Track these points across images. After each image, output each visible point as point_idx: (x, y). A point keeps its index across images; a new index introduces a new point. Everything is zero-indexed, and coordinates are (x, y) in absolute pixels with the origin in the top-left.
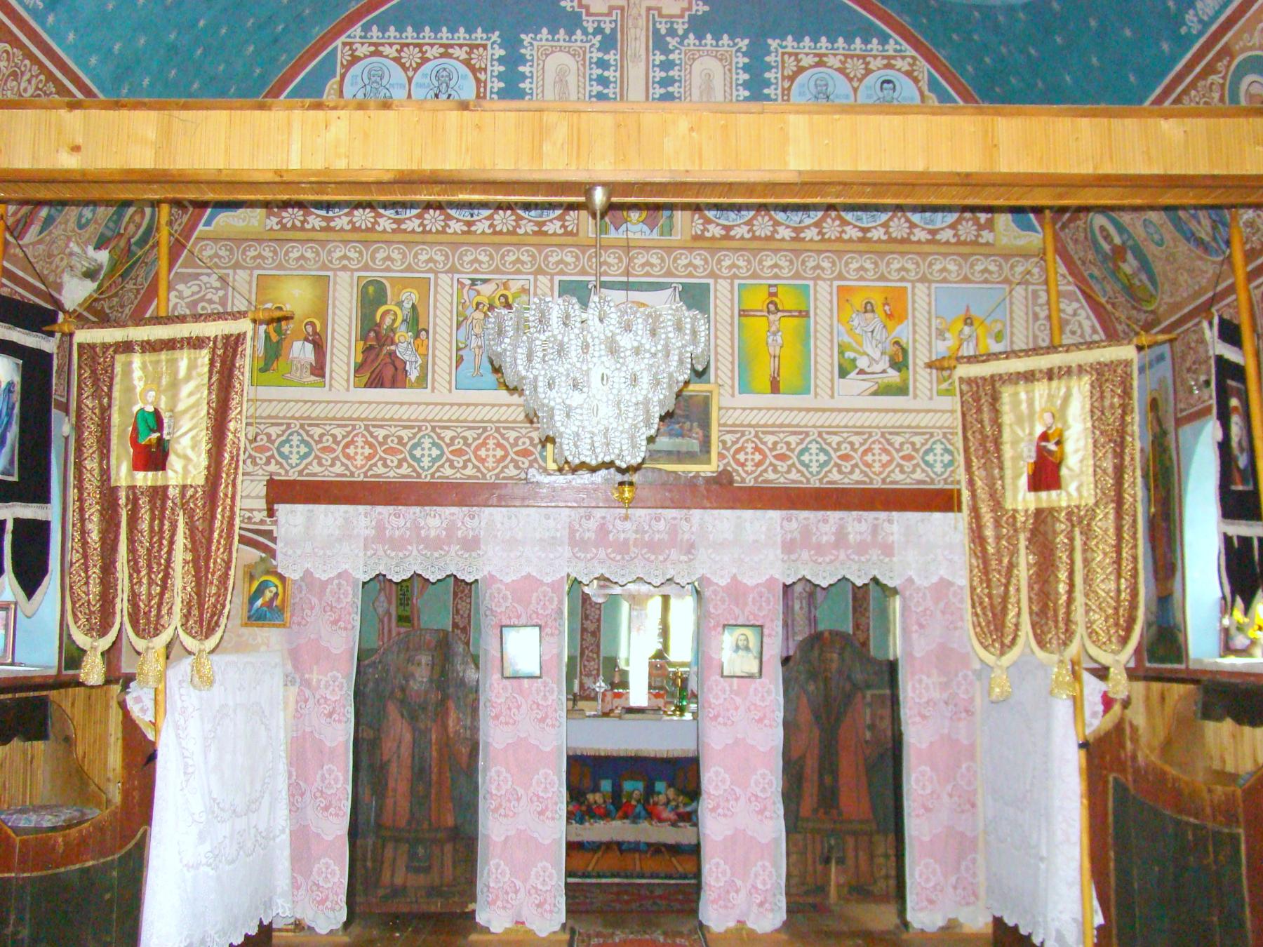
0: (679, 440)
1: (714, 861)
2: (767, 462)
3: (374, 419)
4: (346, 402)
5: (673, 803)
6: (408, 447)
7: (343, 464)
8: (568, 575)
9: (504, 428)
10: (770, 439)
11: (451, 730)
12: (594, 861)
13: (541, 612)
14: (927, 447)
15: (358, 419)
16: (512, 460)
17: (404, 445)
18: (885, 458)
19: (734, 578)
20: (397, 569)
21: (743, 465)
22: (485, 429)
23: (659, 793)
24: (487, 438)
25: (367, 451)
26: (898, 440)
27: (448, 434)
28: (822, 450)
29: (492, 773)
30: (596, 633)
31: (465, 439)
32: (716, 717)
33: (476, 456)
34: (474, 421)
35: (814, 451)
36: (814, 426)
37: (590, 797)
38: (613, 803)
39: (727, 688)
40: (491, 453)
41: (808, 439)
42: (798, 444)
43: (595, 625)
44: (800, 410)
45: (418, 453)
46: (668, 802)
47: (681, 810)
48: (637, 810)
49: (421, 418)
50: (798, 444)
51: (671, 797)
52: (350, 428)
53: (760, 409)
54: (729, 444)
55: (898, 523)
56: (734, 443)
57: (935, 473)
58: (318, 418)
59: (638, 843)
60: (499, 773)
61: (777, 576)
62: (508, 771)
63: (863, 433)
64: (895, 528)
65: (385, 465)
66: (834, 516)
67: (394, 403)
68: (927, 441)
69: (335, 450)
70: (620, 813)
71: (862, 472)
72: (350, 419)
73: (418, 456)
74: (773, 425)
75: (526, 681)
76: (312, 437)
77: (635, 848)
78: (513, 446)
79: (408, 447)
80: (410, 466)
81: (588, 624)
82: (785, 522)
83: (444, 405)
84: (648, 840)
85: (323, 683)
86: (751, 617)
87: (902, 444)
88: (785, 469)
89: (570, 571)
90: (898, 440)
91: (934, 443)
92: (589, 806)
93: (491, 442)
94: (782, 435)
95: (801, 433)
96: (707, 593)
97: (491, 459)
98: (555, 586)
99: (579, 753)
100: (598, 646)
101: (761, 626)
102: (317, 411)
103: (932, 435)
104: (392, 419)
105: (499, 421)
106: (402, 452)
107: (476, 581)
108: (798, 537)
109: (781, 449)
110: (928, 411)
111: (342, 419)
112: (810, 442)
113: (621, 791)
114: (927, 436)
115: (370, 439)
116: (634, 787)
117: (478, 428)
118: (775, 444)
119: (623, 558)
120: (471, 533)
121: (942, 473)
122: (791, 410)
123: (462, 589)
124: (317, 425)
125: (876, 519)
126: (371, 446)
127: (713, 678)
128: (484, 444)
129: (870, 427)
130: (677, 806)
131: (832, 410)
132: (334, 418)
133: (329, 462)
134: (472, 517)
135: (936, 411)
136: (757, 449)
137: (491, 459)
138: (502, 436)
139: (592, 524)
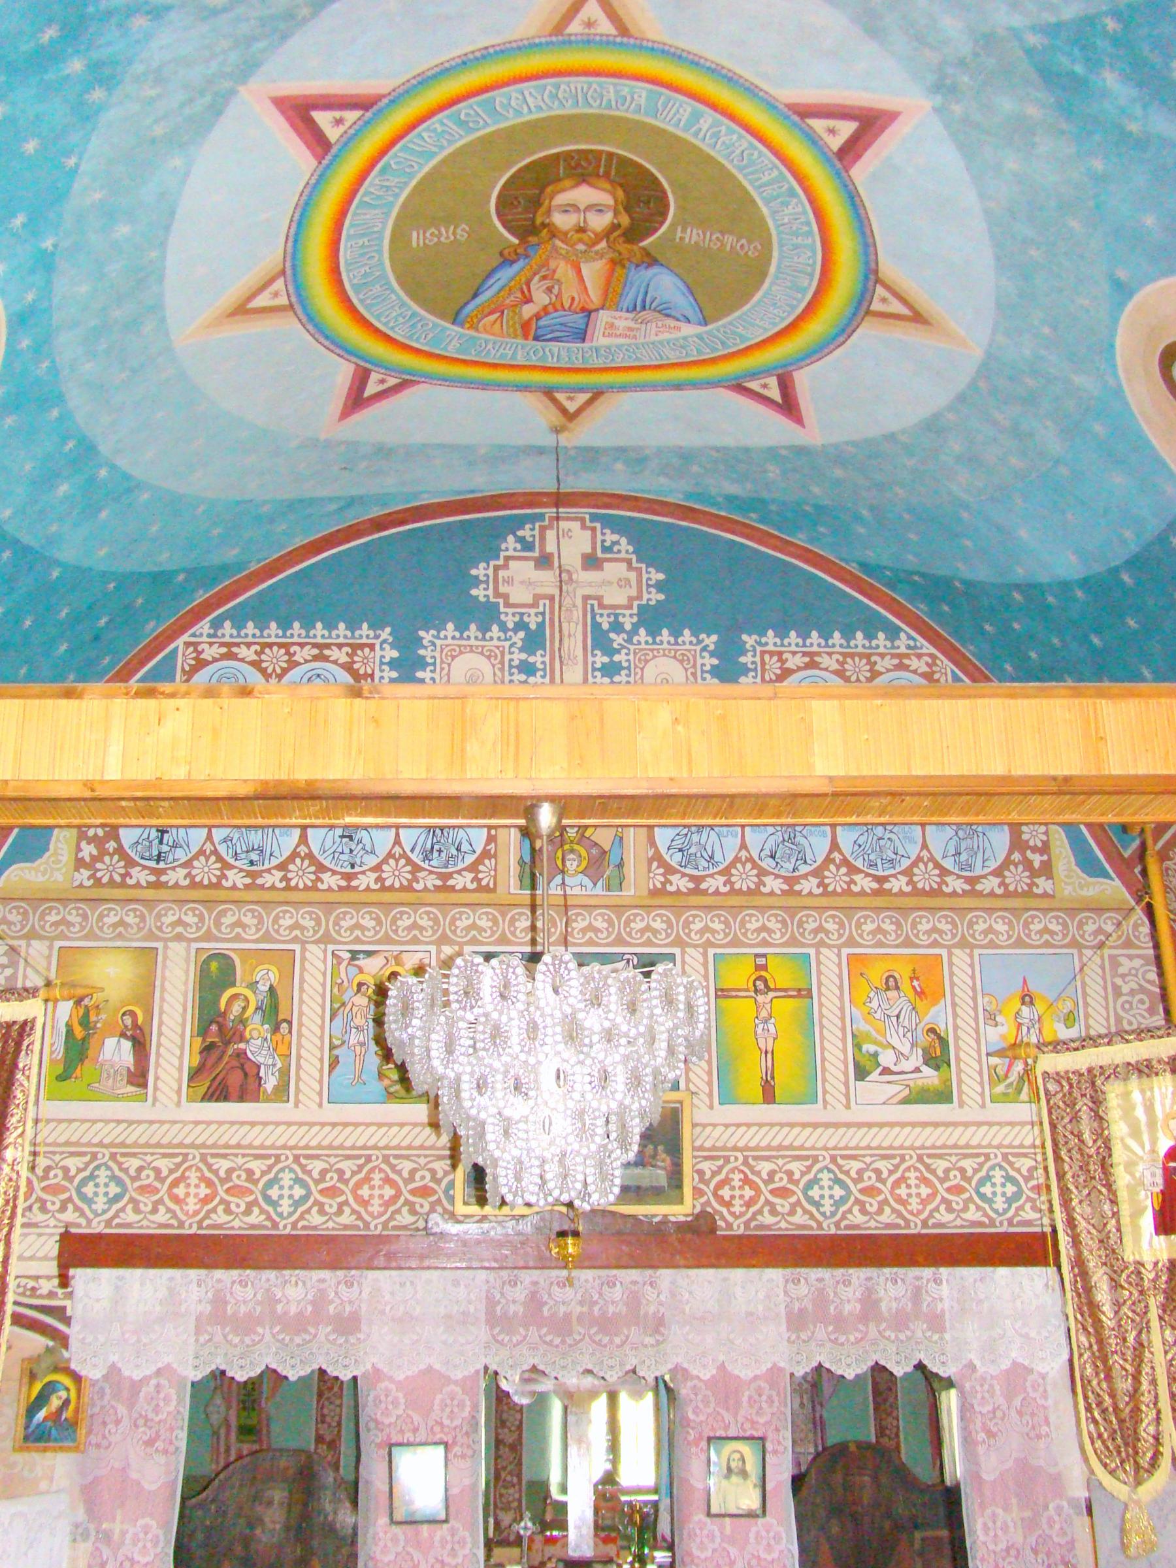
4: (175, 1122)
6: (260, 1185)
9: (396, 1157)
10: (765, 1167)
13: (446, 1422)
18: (925, 1191)
19: (722, 1367)
20: (242, 1362)
21: (728, 1204)
24: (372, 1170)
25: (204, 1191)
26: (940, 1165)
27: (317, 1166)
28: (837, 1181)
30: (516, 1447)
35: (826, 1183)
39: (717, 1533)
40: (377, 1192)
43: (515, 1436)
44: (804, 1125)
45: (274, 1193)
50: (803, 1174)
54: (708, 1175)
55: (949, 1284)
61: (782, 1364)
63: (893, 1157)
64: (945, 1290)
65: (228, 1211)
67: (243, 1123)
68: (981, 1165)
69: (157, 1191)
71: (894, 1210)
72: (181, 1145)
73: (275, 1198)
76: (126, 1171)
85: (129, 1536)
86: (748, 1425)
87: (947, 1171)
90: (940, 1165)
91: (992, 1168)
93: (377, 1177)
94: (780, 1162)
95: (807, 1158)
97: (376, 1202)
100: (520, 1464)
101: (763, 1439)
102: (135, 1135)
103: (987, 1157)
105: (386, 1147)
106: (251, 1192)
108: (810, 1308)
109: (781, 1181)
110: (979, 1124)
111: (170, 1145)
112: (821, 1170)
117: (358, 1157)
118: (772, 1174)
119: (563, 1342)
120: (348, 1309)
122: (792, 1125)
124: (134, 1155)
126: (209, 1183)
128: (367, 1179)
132: (158, 1145)
134: (349, 1284)
136: (746, 1181)
137: (376, 1202)
139: (520, 1293)
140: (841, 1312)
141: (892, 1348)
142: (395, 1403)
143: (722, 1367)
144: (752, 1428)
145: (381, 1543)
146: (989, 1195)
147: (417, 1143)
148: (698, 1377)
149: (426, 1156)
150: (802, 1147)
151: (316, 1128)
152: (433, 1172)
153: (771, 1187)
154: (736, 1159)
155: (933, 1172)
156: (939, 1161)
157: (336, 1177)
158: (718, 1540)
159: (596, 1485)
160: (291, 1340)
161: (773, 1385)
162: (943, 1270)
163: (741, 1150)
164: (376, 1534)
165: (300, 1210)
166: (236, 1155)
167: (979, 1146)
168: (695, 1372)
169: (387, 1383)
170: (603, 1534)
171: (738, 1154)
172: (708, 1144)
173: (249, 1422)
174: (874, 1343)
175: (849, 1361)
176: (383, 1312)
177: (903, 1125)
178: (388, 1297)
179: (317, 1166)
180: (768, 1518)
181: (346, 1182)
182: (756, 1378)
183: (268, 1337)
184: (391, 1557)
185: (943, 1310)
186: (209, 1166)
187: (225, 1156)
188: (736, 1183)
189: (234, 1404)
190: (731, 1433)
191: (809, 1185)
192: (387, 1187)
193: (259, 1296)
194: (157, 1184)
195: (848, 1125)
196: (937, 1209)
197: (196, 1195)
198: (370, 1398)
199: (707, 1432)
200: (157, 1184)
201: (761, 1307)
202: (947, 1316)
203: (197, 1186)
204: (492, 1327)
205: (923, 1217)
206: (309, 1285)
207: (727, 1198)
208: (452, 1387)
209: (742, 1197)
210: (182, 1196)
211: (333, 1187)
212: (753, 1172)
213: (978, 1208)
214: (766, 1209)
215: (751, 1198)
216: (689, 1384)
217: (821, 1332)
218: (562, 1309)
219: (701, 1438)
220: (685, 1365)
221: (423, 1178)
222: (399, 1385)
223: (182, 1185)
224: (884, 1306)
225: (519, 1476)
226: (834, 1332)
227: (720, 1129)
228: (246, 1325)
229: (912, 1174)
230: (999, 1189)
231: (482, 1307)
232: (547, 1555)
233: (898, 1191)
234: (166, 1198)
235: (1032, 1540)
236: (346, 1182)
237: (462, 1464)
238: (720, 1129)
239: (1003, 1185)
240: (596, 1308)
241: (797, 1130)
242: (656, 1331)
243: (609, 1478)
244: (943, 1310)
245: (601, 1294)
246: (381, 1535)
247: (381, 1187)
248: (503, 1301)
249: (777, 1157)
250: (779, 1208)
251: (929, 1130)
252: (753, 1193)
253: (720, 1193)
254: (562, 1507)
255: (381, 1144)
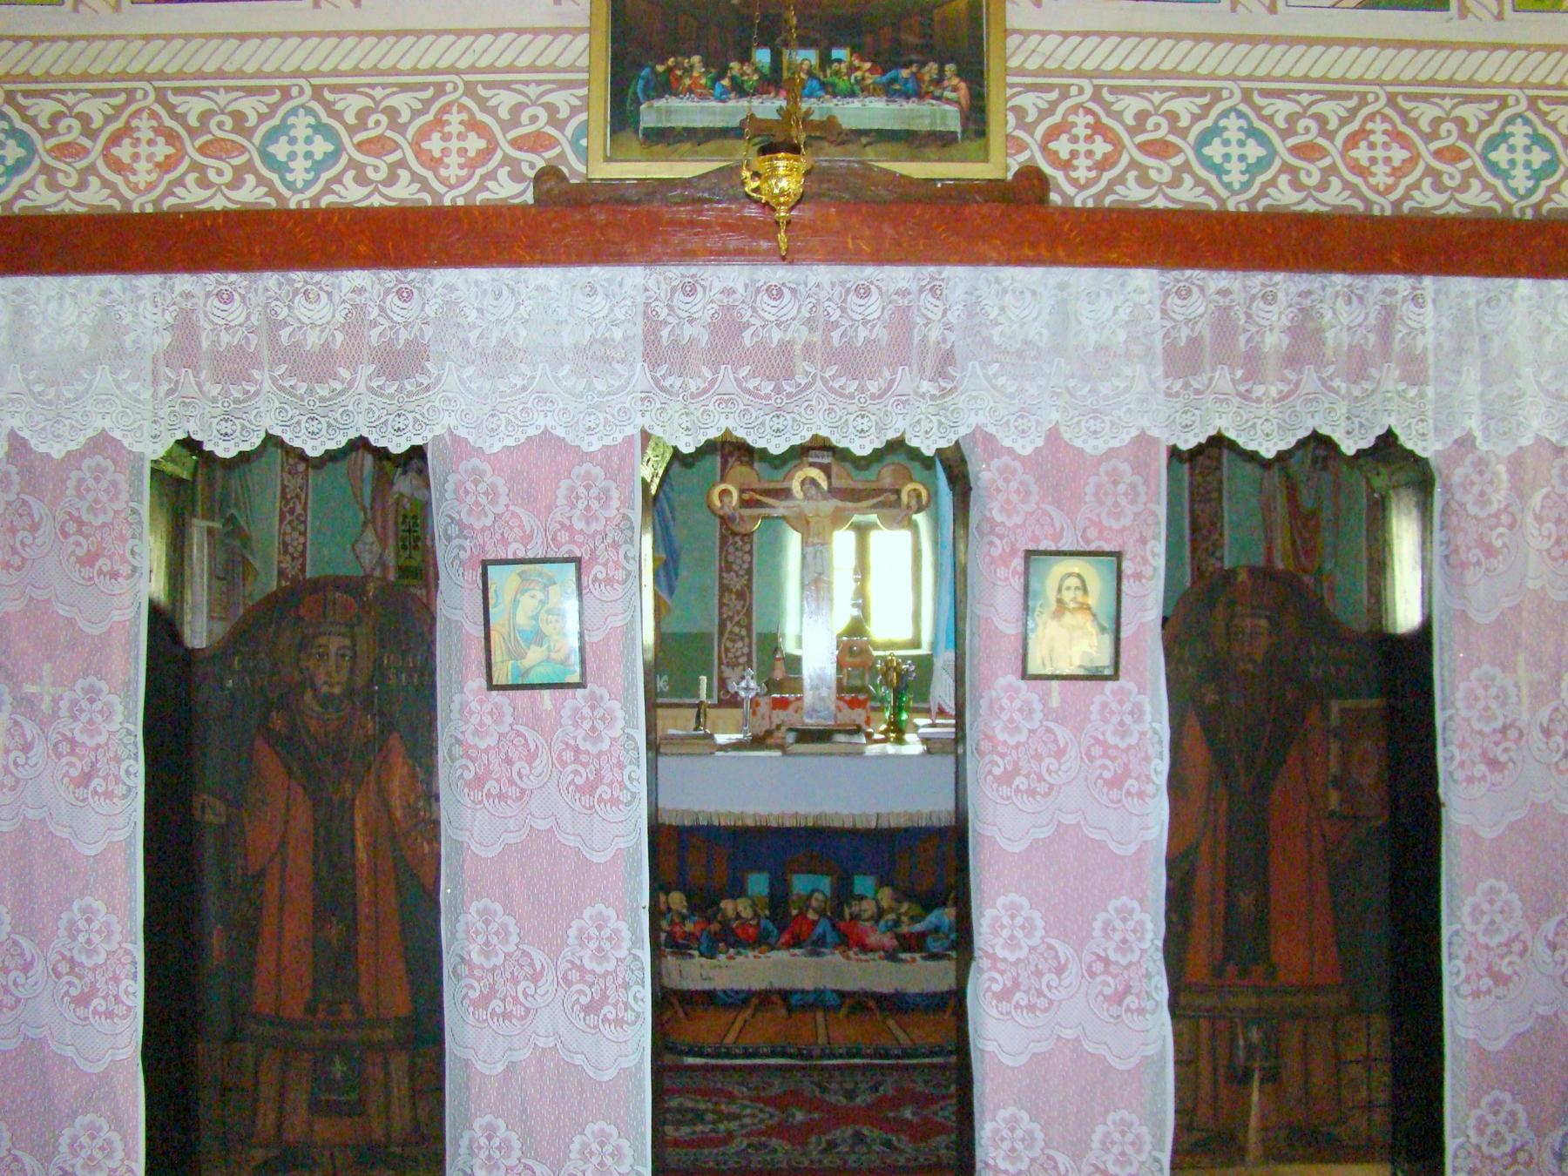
0: (911, 106)
1: (1003, 1114)
2: (1124, 160)
3: (181, 75)
4: (113, 38)
5: (891, 916)
6: (257, 139)
7: (106, 183)
8: (646, 437)
9: (488, 85)
10: (1130, 106)
11: (396, 802)
12: (738, 1025)
13: (579, 525)
14: (1494, 129)
15: (141, 76)
16: (507, 160)
17: (250, 134)
18: (1399, 155)
19: (1053, 436)
20: (226, 427)
21: (1066, 166)
22: (440, 90)
23: (862, 898)
24: (446, 109)
25: (162, 150)
26: (1426, 113)
27: (351, 105)
28: (1252, 132)
29: (472, 915)
30: (744, 594)
31: (393, 113)
32: (1007, 778)
33: (419, 154)
34: (415, 71)
35: (1233, 135)
36: (1232, 77)
37: (727, 906)
38: (772, 919)
39: (1038, 706)
40: (454, 144)
41: (1220, 107)
42: (1196, 118)
43: (744, 581)
44: (1198, 38)
45: (280, 150)
46: (881, 913)
47: (904, 929)
48: (819, 930)
49: (287, 68)
50: (1196, 118)
51: (885, 904)
52: (121, 99)
53: (1104, 35)
54: (1032, 116)
55: (1436, 304)
56: (1044, 114)
57: (1513, 191)
58: (48, 77)
59: (820, 993)
60: (487, 916)
61: (1154, 433)
62: (509, 910)
63: (1348, 96)
64: (1429, 316)
65: (204, 183)
66: (1287, 285)
67: (226, 36)
68: (1492, 115)
69: (87, 151)
70: (786, 937)
71: (1347, 185)
72: (122, 76)
73: (282, 157)
74: (1136, 73)
75: (546, 693)
76: (32, 121)
77: (815, 1002)
78: (506, 126)
79: (257, 139)
80: (261, 181)
81: (730, 578)
82: (1173, 300)
83: (342, 35)
84: (838, 987)
85: (64, 704)
86: (1092, 533)
87: (1436, 122)
88: (1167, 176)
89: (646, 422)
90: (1426, 113)
91: (1510, 121)
92: (725, 924)
93: (455, 119)
94: (1157, 97)
95: (1202, 92)
96: (983, 473)
97: (453, 160)
98: (614, 461)
99: (703, 822)
100: (749, 613)
101: (1118, 555)
102: (46, 60)
103: (1503, 102)
104: (220, 74)
105: (473, 69)
106: (243, 150)
107: (418, 453)
108: (1207, 334)
109: (1158, 129)
110: (1494, 47)
111: (102, 77)
112: (1224, 114)
113: (786, 894)
114: (1494, 105)
115: (169, 122)
116: (811, 886)
117: (423, 87)
118: (1142, 116)
119: (778, 390)
120: (404, 335)
121: (1531, 192)
122: (1178, 37)
123: (392, 479)
124: (45, 94)
125: (1391, 292)
126: (171, 138)
127: (1002, 682)
128: (439, 122)
129: (1360, 81)
130: (897, 923)
131: (1273, 40)
132: (85, 77)
133: (74, 180)
134: (405, 295)
135: (1512, 48)
136: (1098, 128)
137: (453, 160)
138: (482, 103)
139: (703, 308)
140: (1257, 348)
141: (1342, 408)
142: (492, 494)
143: (1053, 436)
144: (1101, 537)
145: (475, 720)
146: (1504, 165)
147: (524, 61)
148: (1010, 451)
149: (539, 83)
150: (1193, 75)
151: (350, 42)
152: (552, 109)
153: (1139, 139)
154: (1081, 91)
155: (1413, 124)
156: (1423, 107)
157: (384, 120)
158: (1038, 715)
159: (839, 636)
160: (311, 391)
161: (1140, 467)
162: (1428, 281)
163: (1089, 76)
164: (464, 705)
165: (325, 176)
166: (215, 90)
167: (1489, 84)
168: (1007, 443)
169: (476, 461)
170: (848, 697)
171: (1085, 83)
172: (1031, 65)
173: (413, 563)
174: (1312, 399)
175: (1267, 427)
176: (465, 343)
177: (1365, 43)
178: (473, 315)
179: (351, 105)
180: (1122, 682)
181: (402, 129)
182: (1111, 453)
183: (267, 384)
184: (492, 741)
185: (1425, 349)
186: (171, 109)
187: (196, 92)
188: (1081, 131)
189: (391, 542)
190: (1065, 545)
191: (1204, 139)
192: (472, 135)
193: (254, 320)
194: (87, 143)
195: (1273, 40)
196: (1416, 186)
197: (150, 158)
198: (450, 486)
199: (1025, 544)
200: (87, 143)
201: (1122, 335)
202: (1431, 359)
203: (151, 142)
204: (654, 366)
205: (1394, 196)
206: (337, 298)
207: (1064, 155)
208: (587, 466)
209: (1090, 153)
210: (126, 160)
211: (381, 137)
212: (1109, 114)
213: (1486, 186)
214: (1131, 175)
215: (1106, 156)
216: (995, 463)
217: (1223, 379)
218: (776, 335)
219: (1013, 553)
220: (991, 429)
221: (534, 119)
222: (493, 459)
223: (126, 142)
224: (1329, 335)
225: (749, 628)
226: (1245, 380)
227: (1054, 40)
228: (235, 367)
229: (1378, 126)
230: (1520, 157)
231: (639, 329)
232: (776, 721)
233: (1353, 153)
234: (101, 165)
235: (1544, 714)
236: (402, 129)
237: (607, 593)
238: (1054, 40)
239: (1527, 149)
240: (836, 335)
241: (1185, 45)
242: (941, 373)
243: (857, 628)
244: (1425, 349)
245: (843, 310)
246: (474, 706)
247: (461, 137)
248: (673, 320)
249: (1151, 90)
250: (1153, 174)
251: (1408, 53)
252: (1109, 148)
253: (1053, 146)
254: (794, 663)
255: (462, 65)
